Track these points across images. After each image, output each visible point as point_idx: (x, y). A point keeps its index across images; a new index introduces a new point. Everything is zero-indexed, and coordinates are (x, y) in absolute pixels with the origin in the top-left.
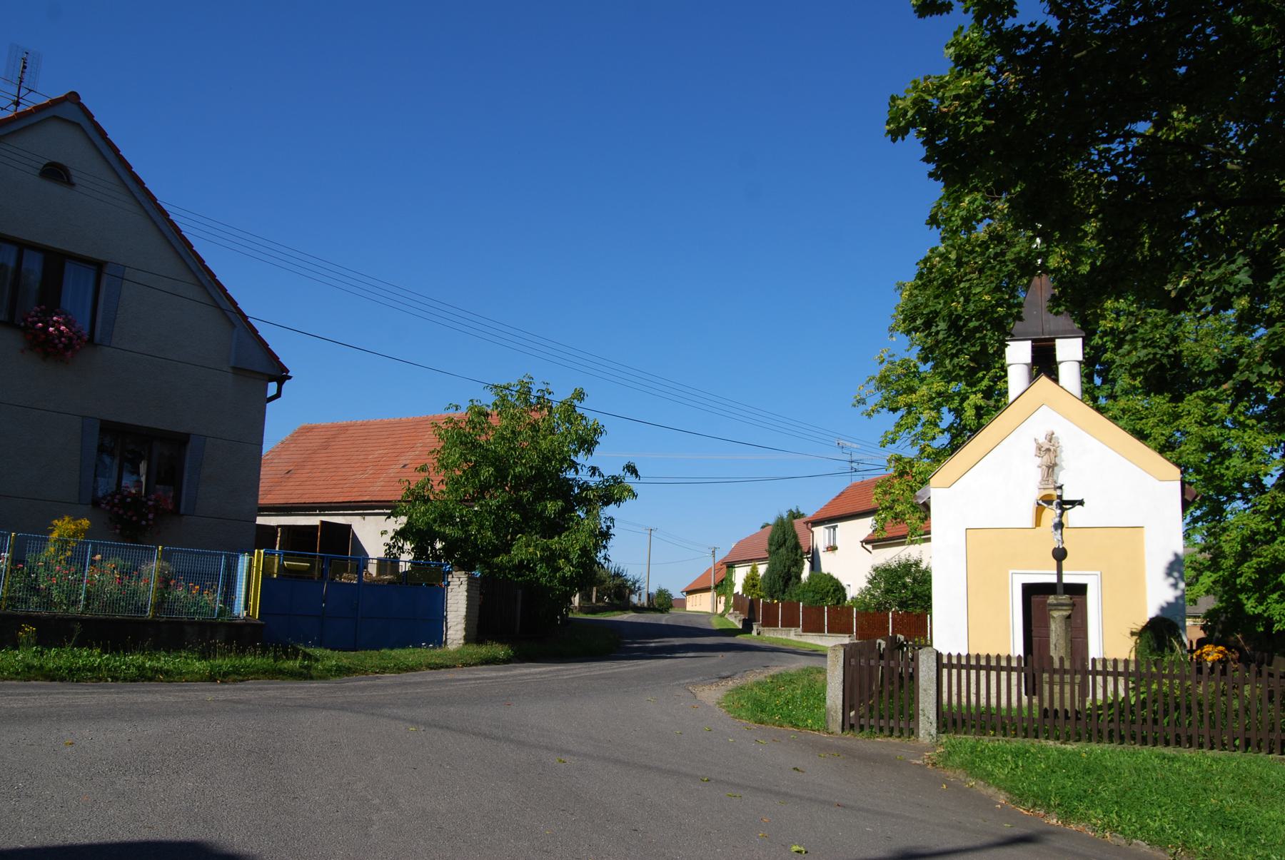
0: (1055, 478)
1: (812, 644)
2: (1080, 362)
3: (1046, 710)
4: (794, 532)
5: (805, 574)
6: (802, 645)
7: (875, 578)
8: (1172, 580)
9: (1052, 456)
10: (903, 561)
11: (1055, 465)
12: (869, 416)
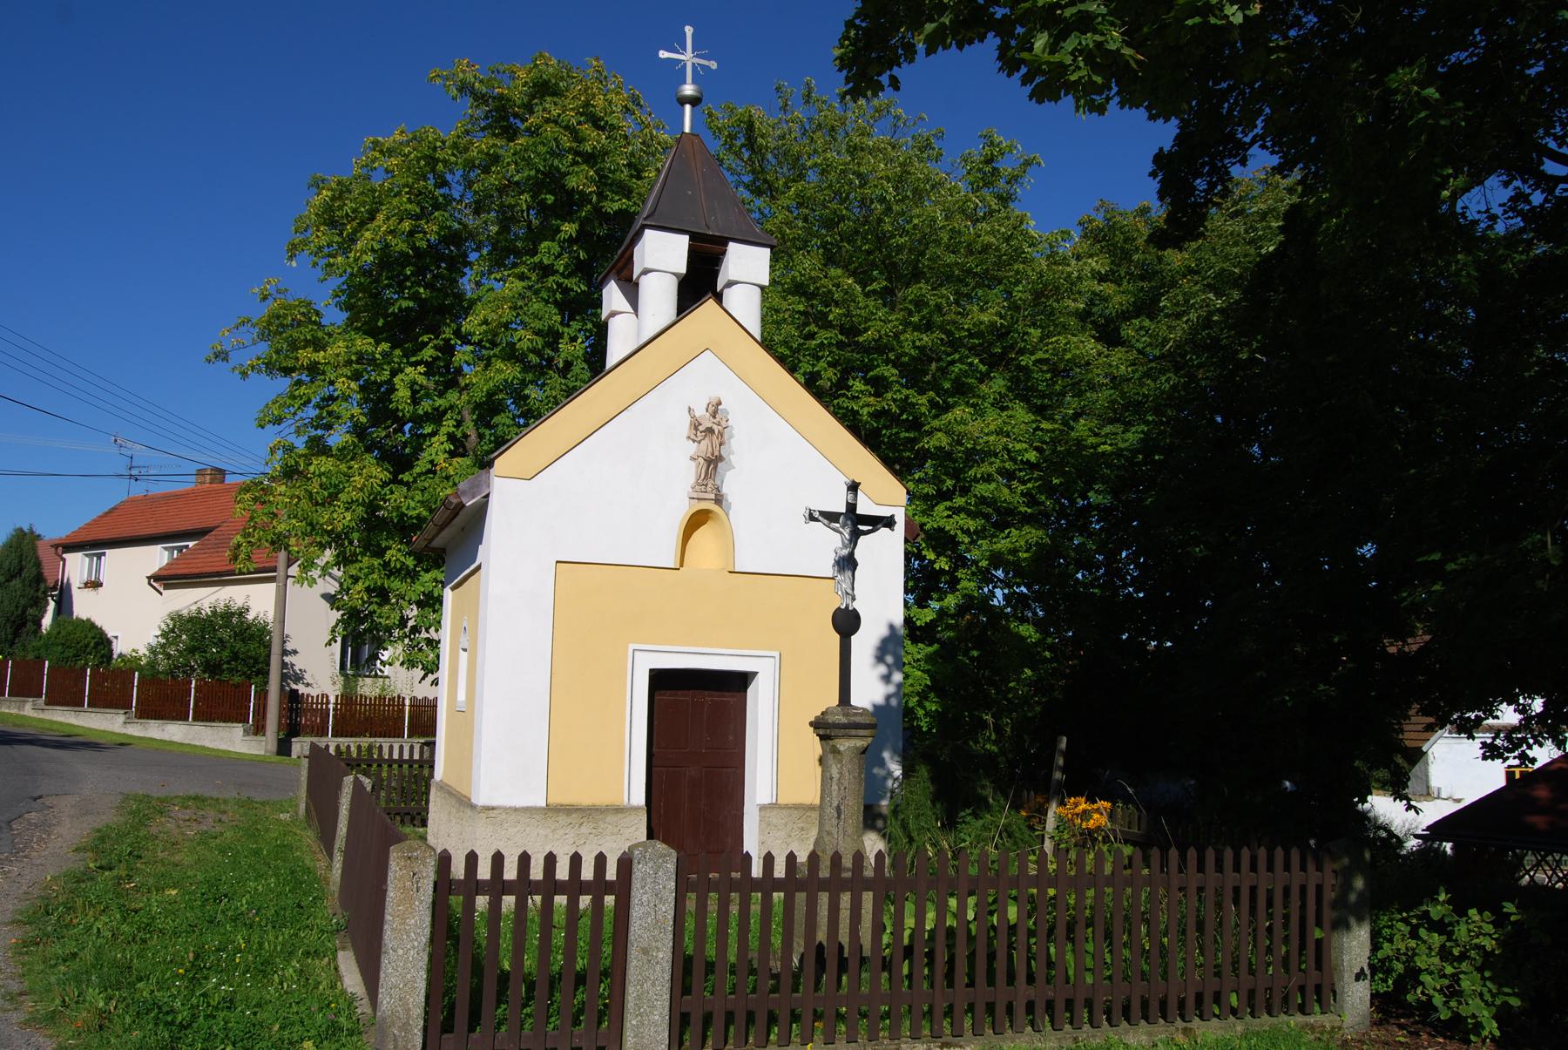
0: (718, 482)
1: (61, 724)
2: (762, 288)
3: (820, 946)
4: (37, 558)
5: (47, 621)
6: (47, 726)
7: (172, 631)
8: (882, 669)
9: (716, 442)
10: (221, 608)
11: (720, 458)
12: (244, 374)
